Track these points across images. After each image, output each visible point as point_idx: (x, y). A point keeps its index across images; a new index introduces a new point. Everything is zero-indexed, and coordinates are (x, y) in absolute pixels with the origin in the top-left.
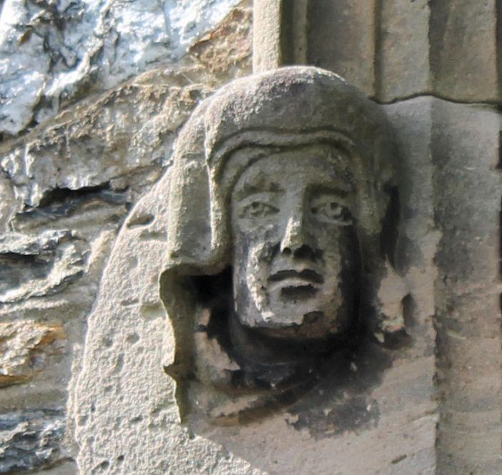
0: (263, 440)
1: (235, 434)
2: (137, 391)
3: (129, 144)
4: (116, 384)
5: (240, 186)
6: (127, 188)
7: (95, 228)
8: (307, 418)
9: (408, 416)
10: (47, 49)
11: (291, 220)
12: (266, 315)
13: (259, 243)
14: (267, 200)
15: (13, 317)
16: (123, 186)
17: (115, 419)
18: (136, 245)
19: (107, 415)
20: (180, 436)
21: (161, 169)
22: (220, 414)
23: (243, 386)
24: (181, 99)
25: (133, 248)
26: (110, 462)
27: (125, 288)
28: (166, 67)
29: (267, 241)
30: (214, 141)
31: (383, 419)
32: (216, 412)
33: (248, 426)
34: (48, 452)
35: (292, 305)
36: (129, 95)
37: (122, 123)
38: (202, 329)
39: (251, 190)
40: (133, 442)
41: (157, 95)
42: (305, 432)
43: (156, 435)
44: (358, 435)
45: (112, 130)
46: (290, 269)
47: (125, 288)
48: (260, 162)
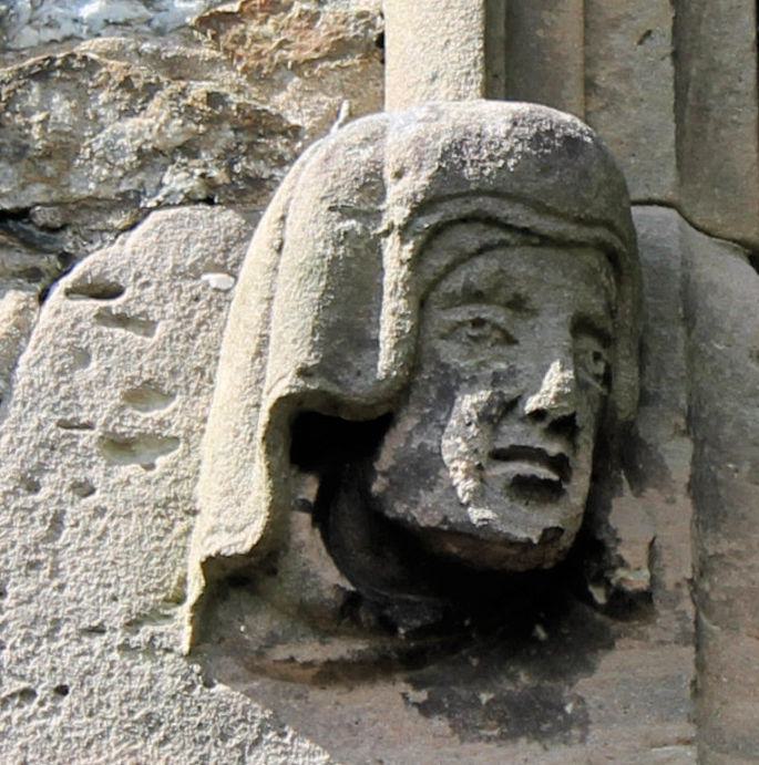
0: (355, 719)
1: (298, 697)
2: (96, 581)
3: (78, 154)
4: (51, 559)
5: (455, 283)
6: (64, 227)
8: (445, 700)
9: (647, 738)
11: (556, 365)
12: (476, 515)
13: (480, 389)
14: (501, 320)
16: (58, 222)
17: (49, 619)
18: (88, 330)
19: (32, 609)
20: (185, 677)
21: (135, 210)
22: (287, 657)
23: (355, 620)
24: (189, 101)
25: (81, 333)
26: (39, 692)
27: (65, 398)
28: (145, 40)
29: (497, 390)
30: (420, 197)
33: (324, 688)
35: (522, 509)
36: (79, 70)
37: (64, 115)
38: (305, 506)
39: (474, 296)
40: (86, 667)
41: (138, 84)
42: (440, 724)
43: (133, 665)
44: (546, 749)
45: (44, 122)
46: (537, 446)
47: (65, 398)
48: (499, 253)
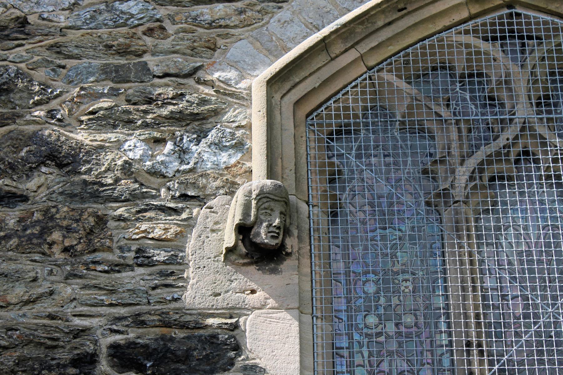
5: (263, 207)
7: (194, 207)
10: (179, 158)
12: (266, 241)
15: (170, 224)
31: (283, 273)
32: (237, 261)
34: (181, 261)
38: (240, 240)
39: (265, 209)
42: (260, 272)
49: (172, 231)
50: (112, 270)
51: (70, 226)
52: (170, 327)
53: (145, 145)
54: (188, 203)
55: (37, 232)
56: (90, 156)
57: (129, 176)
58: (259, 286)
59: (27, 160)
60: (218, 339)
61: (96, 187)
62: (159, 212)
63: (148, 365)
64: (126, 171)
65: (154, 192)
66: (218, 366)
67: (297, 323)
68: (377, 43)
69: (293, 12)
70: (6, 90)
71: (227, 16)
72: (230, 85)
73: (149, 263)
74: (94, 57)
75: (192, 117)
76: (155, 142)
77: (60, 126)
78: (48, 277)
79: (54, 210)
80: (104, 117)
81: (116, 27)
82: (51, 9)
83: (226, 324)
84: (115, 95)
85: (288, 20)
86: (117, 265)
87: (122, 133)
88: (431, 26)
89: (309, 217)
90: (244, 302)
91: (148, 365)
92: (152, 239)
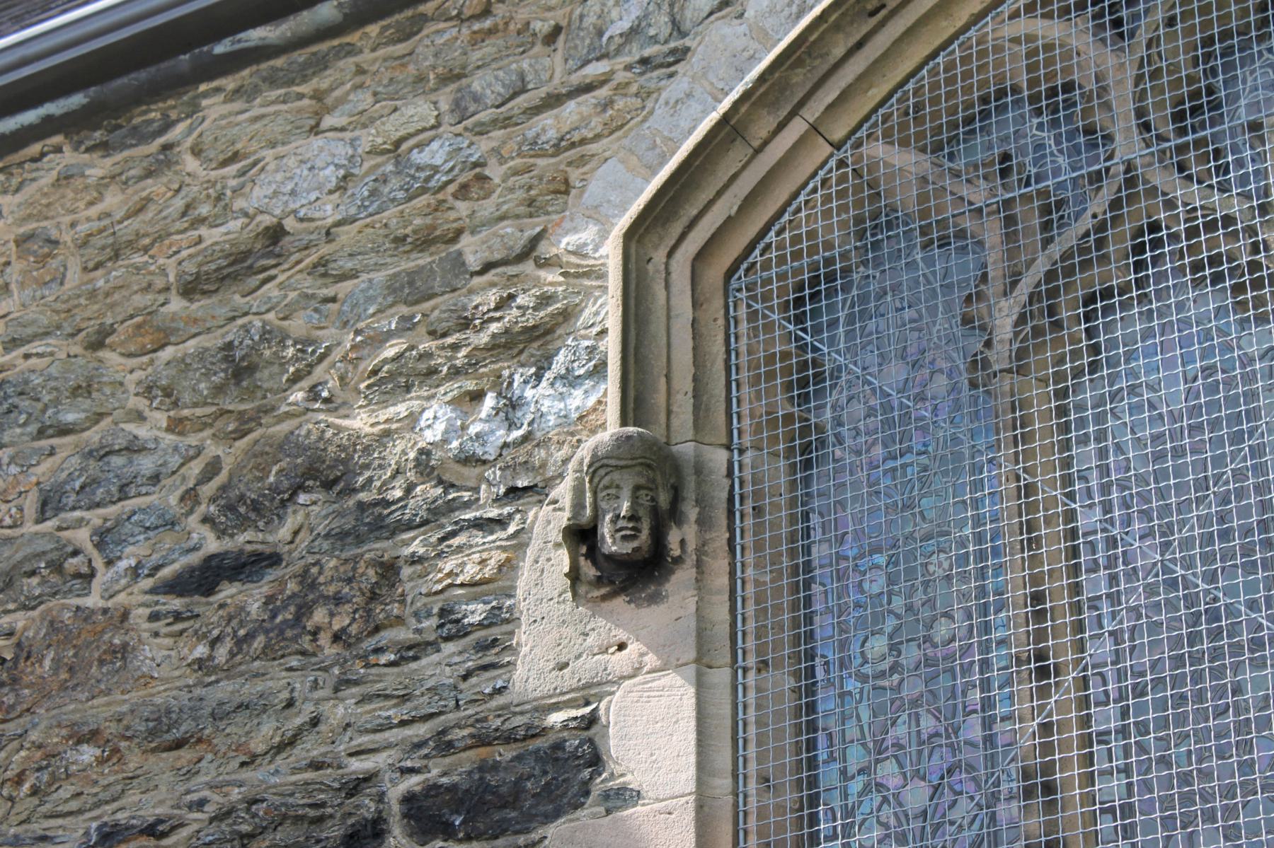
10: (507, 419)
12: (614, 548)
15: (491, 549)
39: (607, 487)
42: (633, 605)
49: (492, 562)
50: (402, 658)
51: (339, 592)
52: (490, 744)
53: (453, 410)
54: (521, 501)
55: (290, 617)
56: (370, 455)
57: (428, 475)
58: (630, 632)
59: (277, 488)
60: (564, 749)
61: (378, 510)
62: (475, 532)
63: (457, 823)
64: (422, 467)
65: (466, 495)
66: (565, 800)
67: (692, 691)
68: (838, 93)
69: (693, 78)
70: (247, 368)
71: (585, 121)
72: (585, 256)
73: (458, 631)
74: (378, 267)
75: (527, 336)
76: (472, 399)
77: (328, 410)
78: (310, 695)
79: (314, 570)
80: (392, 376)
81: (410, 199)
82: (313, 197)
83: (575, 719)
84: (409, 329)
85: (682, 95)
86: (410, 648)
87: (418, 398)
88: (944, 24)
89: (730, 474)
90: (605, 669)
91: (457, 823)
92: (462, 585)
